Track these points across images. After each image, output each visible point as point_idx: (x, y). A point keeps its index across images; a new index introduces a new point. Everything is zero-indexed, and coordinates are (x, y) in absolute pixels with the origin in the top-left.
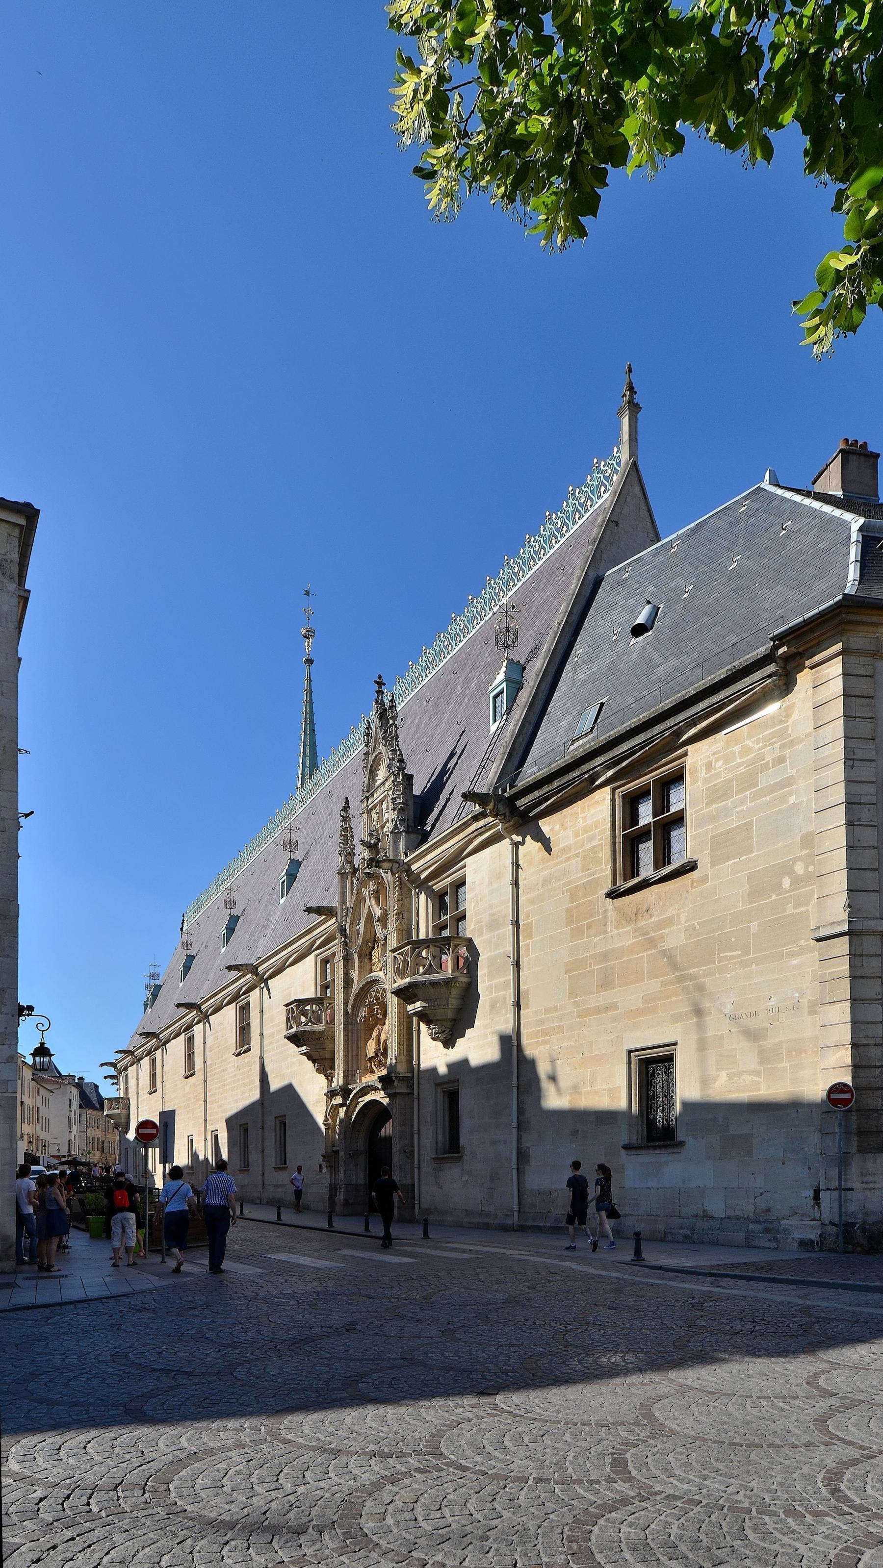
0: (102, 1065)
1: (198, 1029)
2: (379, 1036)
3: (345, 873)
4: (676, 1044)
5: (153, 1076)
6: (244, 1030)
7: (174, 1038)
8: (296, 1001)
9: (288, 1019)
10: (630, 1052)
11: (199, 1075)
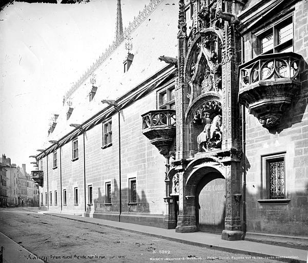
0: (30, 157)
1: (80, 138)
2: (209, 129)
3: (182, 38)
4: (285, 152)
5: (55, 161)
6: (75, 151)
7: (67, 143)
8: (150, 112)
9: (144, 122)
10: (262, 156)
11: (59, 167)
